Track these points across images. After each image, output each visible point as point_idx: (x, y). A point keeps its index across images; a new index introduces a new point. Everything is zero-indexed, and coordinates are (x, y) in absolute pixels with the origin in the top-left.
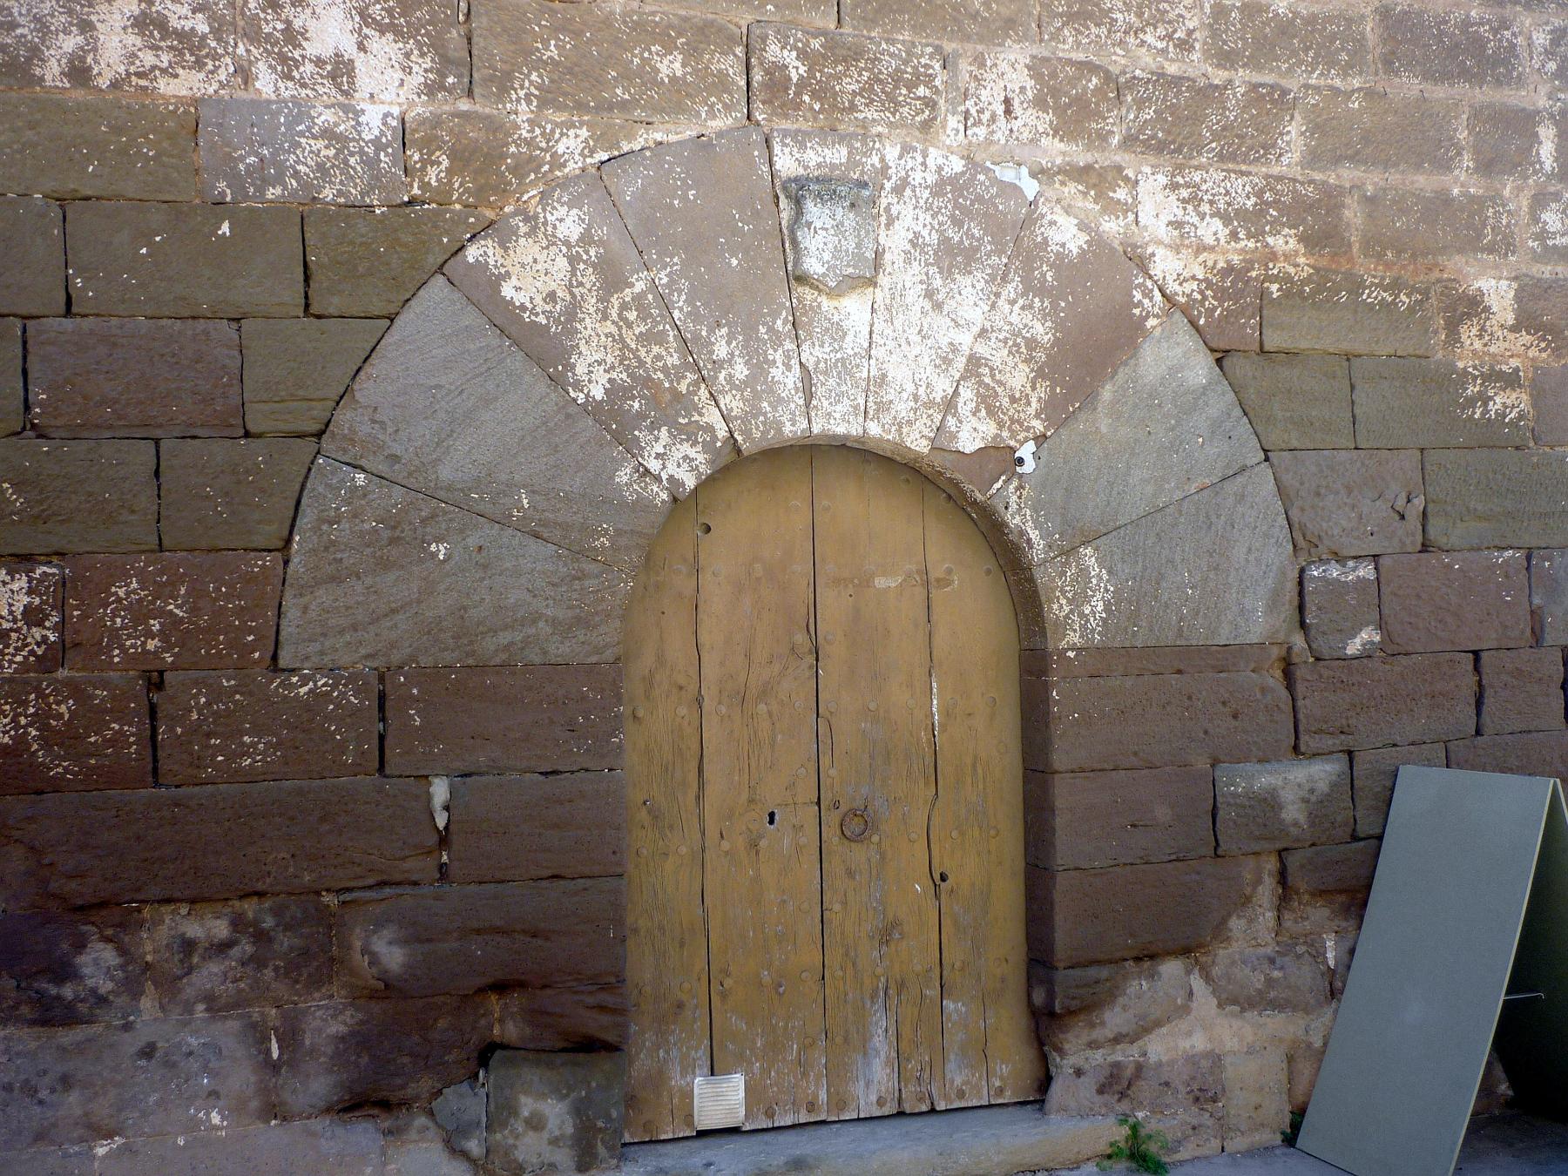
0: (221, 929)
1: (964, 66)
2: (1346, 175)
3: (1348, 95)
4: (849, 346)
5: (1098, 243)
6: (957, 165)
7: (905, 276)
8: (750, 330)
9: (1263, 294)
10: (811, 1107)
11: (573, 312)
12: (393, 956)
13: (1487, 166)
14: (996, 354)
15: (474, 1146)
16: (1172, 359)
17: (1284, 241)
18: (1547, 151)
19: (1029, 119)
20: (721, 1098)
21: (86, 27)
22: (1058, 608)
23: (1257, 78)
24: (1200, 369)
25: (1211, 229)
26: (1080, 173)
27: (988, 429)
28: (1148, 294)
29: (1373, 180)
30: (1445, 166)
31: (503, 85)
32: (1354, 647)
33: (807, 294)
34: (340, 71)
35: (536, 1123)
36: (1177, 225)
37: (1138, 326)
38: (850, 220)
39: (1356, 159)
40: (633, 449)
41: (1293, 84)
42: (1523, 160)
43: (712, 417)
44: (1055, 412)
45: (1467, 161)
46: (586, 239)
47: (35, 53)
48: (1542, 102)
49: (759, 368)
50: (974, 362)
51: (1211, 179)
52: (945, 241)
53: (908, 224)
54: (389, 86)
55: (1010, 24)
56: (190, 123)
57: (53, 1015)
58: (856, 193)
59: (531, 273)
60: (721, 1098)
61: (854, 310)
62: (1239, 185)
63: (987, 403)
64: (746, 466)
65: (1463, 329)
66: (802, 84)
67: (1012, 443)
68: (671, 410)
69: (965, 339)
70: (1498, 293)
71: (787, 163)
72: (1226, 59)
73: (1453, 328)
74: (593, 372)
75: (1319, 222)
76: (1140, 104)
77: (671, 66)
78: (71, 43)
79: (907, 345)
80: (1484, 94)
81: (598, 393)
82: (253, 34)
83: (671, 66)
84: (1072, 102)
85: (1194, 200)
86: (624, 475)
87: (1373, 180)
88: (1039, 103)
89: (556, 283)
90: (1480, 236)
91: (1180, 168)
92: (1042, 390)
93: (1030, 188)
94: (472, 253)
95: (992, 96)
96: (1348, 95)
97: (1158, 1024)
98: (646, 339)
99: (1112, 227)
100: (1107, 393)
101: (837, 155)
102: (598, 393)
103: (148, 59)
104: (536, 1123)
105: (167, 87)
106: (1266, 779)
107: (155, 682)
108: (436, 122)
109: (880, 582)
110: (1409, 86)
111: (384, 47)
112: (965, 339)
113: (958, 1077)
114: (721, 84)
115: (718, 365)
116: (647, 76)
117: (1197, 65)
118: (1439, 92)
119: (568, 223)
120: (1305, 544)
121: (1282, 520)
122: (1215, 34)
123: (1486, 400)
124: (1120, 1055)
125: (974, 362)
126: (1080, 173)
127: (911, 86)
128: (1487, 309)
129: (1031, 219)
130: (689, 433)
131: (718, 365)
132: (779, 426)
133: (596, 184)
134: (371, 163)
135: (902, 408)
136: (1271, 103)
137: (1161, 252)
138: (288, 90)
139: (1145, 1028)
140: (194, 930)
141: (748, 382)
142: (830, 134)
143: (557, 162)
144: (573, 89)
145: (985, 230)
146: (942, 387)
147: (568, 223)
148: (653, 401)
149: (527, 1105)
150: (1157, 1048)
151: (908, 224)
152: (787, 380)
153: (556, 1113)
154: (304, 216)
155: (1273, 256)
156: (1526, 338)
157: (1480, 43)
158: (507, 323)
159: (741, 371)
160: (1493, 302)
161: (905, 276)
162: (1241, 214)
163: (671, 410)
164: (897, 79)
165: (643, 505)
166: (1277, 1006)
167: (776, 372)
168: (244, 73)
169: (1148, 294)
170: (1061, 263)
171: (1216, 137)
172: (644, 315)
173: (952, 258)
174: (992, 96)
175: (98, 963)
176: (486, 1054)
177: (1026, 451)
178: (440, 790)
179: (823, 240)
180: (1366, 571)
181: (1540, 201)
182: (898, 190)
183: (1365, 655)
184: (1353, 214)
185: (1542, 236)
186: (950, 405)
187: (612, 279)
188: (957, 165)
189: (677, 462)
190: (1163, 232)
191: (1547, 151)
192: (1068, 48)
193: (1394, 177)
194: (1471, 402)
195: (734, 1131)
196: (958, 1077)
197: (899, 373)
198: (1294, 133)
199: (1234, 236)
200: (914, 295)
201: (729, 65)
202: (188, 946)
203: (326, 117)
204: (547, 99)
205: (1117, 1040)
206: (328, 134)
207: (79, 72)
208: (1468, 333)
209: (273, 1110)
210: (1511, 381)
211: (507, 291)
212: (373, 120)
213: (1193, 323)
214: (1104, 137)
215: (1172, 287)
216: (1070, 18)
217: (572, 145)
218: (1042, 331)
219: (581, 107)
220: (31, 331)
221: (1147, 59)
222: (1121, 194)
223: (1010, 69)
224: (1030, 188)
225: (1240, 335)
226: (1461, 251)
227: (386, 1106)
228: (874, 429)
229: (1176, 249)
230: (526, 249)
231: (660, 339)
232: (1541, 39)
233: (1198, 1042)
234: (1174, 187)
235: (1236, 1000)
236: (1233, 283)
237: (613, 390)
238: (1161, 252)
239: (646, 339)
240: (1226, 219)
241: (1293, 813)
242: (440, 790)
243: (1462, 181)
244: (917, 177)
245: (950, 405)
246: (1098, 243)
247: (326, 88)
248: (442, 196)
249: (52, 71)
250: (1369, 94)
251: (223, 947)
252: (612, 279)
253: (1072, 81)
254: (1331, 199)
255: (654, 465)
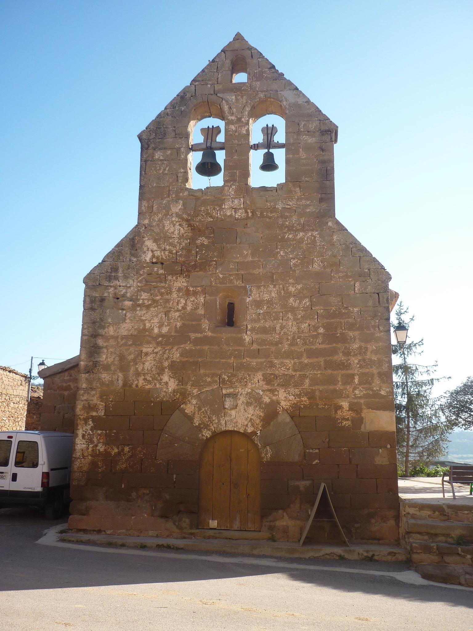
0: (148, 492)
1: (252, 376)
2: (317, 387)
3: (317, 374)
4: (232, 417)
5: (272, 401)
6: (250, 390)
7: (241, 407)
8: (218, 416)
9: (300, 407)
10: (227, 527)
11: (194, 414)
12: (168, 497)
13: (344, 384)
14: (254, 418)
15: (177, 524)
18: (356, 380)
19: (261, 383)
20: (214, 524)
21: (138, 380)
22: (263, 455)
23: (301, 373)
24: (288, 419)
25: (292, 397)
26: (269, 390)
27: (252, 429)
28: (280, 408)
29: (321, 388)
31: (187, 384)
32: (314, 463)
33: (227, 411)
34: (167, 383)
35: (185, 522)
36: (286, 397)
37: (278, 413)
38: (232, 400)
39: (318, 385)
40: (201, 432)
41: (307, 374)
43: (212, 427)
44: (263, 426)
45: (340, 383)
46: (196, 404)
47: (132, 384)
48: (356, 372)
49: (219, 421)
50: (251, 419)
51: (292, 390)
52: (247, 402)
53: (242, 399)
54: (172, 385)
55: (260, 369)
56: (149, 391)
57: (129, 501)
58: (234, 396)
59: (189, 409)
60: (214, 524)
61: (233, 412)
63: (253, 425)
64: (216, 435)
65: (338, 412)
66: (227, 381)
68: (207, 427)
69: (250, 416)
70: (345, 405)
71: (224, 392)
72: (295, 371)
73: (336, 412)
74: (197, 422)
75: (311, 396)
76: (280, 379)
77: (209, 379)
78: (136, 382)
79: (241, 417)
80: (344, 372)
81: (197, 424)
82: (157, 380)
83: (209, 379)
84: (268, 380)
85: (289, 393)
86: (200, 435)
87: (321, 388)
88: (263, 380)
89: (192, 410)
90: (342, 395)
91: (286, 388)
92: (261, 423)
93: (261, 393)
94: (182, 406)
95: (256, 380)
96: (317, 374)
97: (278, 520)
98: (204, 417)
99: (274, 398)
100: (272, 423)
101: (232, 390)
102: (197, 424)
103: (145, 384)
104: (185, 522)
105: (146, 387)
106: (297, 483)
107: (142, 460)
108: (178, 389)
109: (241, 450)
110: (329, 372)
111: (172, 380)
112: (250, 416)
113: (250, 525)
114: (216, 381)
115: (213, 420)
116: (206, 381)
117: (291, 372)
118: (335, 372)
119: (194, 402)
120: (305, 446)
121: (302, 443)
122: (294, 367)
123: (342, 423)
124: (272, 524)
125: (251, 419)
126: (269, 390)
127: (243, 379)
128: (343, 408)
129: (261, 397)
130: (209, 430)
131: (213, 420)
132: (221, 429)
133: (198, 397)
134: (170, 395)
135: (240, 426)
136: (303, 377)
137: (282, 402)
138: (160, 386)
139: (274, 521)
140: (145, 492)
141: (218, 423)
142: (231, 387)
143: (193, 394)
144: (196, 384)
145: (254, 400)
146: (246, 423)
147: (194, 402)
148: (204, 426)
149: (184, 519)
150: (277, 523)
151: (242, 399)
152: (223, 422)
153: (187, 521)
154: (162, 402)
155: (302, 401)
156: (351, 412)
157: (344, 363)
158: (186, 415)
159: (217, 421)
161: (241, 407)
162: (297, 395)
163: (207, 427)
164: (241, 378)
165: (202, 439)
166: (299, 519)
167: (221, 421)
168: (155, 384)
169: (280, 408)
170: (266, 404)
171: (293, 383)
172: (204, 414)
173: (248, 404)
174: (256, 380)
175: (134, 494)
176: (179, 512)
177: (259, 432)
178: (175, 476)
179: (228, 403)
180: (317, 451)
181: (355, 389)
182: (241, 395)
184: (317, 393)
185: (355, 395)
186: (247, 425)
187: (200, 409)
188: (250, 390)
189: (207, 434)
190: (283, 398)
191: (356, 380)
192: (269, 371)
193: (325, 387)
194: (339, 423)
195: (215, 529)
196: (250, 525)
197: (239, 421)
198: (307, 381)
199: (295, 398)
200: (242, 410)
201: (217, 379)
202: (144, 493)
203: (165, 390)
204: (192, 385)
205: (271, 521)
206: (165, 392)
207: (137, 386)
208: (339, 412)
209: (152, 516)
210: (347, 419)
211: (186, 411)
212: (170, 389)
213: (287, 412)
214: (274, 385)
215: (284, 407)
216: (269, 367)
217: (195, 391)
218: (262, 414)
219: (197, 386)
221: (282, 372)
222: (276, 393)
223: (259, 376)
224: (261, 393)
225: (296, 413)
226: (338, 398)
227: (167, 517)
228: (235, 429)
229: (285, 401)
230: (189, 405)
231: (206, 417)
233: (285, 523)
234: (285, 391)
235: (291, 518)
236: (295, 406)
237: (199, 424)
238: (282, 402)
239: (204, 417)
240: (294, 396)
241: (302, 489)
242: (175, 476)
243: (339, 386)
244: (243, 393)
245: (247, 425)
246: (272, 401)
247: (165, 386)
248: (178, 399)
249: (134, 386)
250: (321, 374)
251: (148, 494)
252: (200, 409)
253: (269, 377)
254: (313, 392)
255: (204, 434)
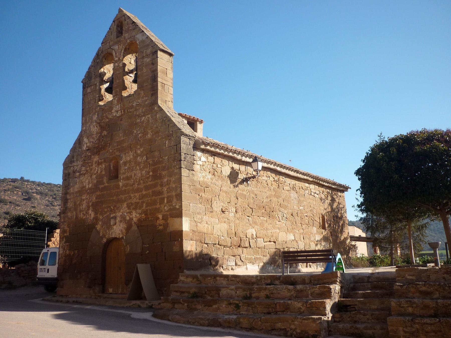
2: (149, 207)
7: (118, 224)
11: (232, 168)
13: (160, 204)
16: (135, 228)
18: (165, 201)
24: (136, 228)
44: (126, 233)
53: (118, 219)
61: (115, 227)
62: (140, 211)
74: (101, 234)
77: (106, 210)
83: (106, 210)
111: (93, 212)
117: (138, 201)
118: (156, 198)
120: (143, 244)
142: (114, 213)
173: (121, 221)
179: (112, 222)
189: (105, 240)
191: (165, 201)
198: (145, 205)
201: (109, 209)
208: (158, 221)
210: (161, 225)
225: (140, 224)
232: (166, 189)
236: (139, 220)
243: (158, 206)
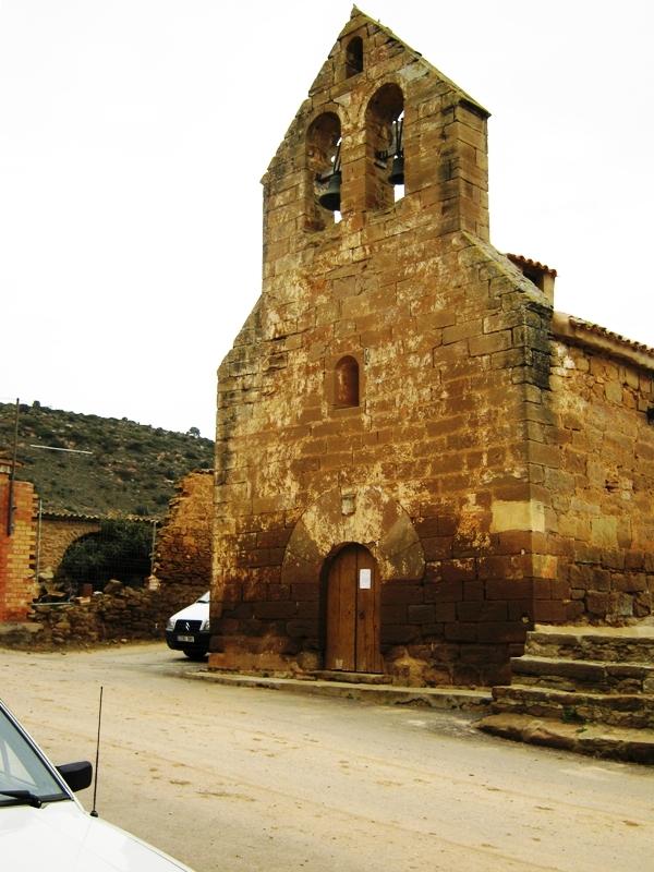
13: (471, 467)
17: (426, 493)
18: (485, 461)
25: (412, 493)
29: (444, 476)
30: (460, 469)
39: (441, 472)
41: (429, 458)
42: (479, 463)
45: (466, 467)
53: (361, 500)
67: (444, 404)
80: (470, 450)
87: (444, 476)
95: (374, 474)
110: (453, 452)
111: (295, 483)
136: (424, 463)
149: (565, 410)
152: (342, 532)
160: (470, 499)
174: (374, 474)
181: (483, 473)
183: (439, 582)
191: (485, 461)
197: (358, 529)
198: (429, 469)
215: (405, 507)
220: (353, 666)
223: (378, 468)
232: (485, 433)
243: (465, 472)
